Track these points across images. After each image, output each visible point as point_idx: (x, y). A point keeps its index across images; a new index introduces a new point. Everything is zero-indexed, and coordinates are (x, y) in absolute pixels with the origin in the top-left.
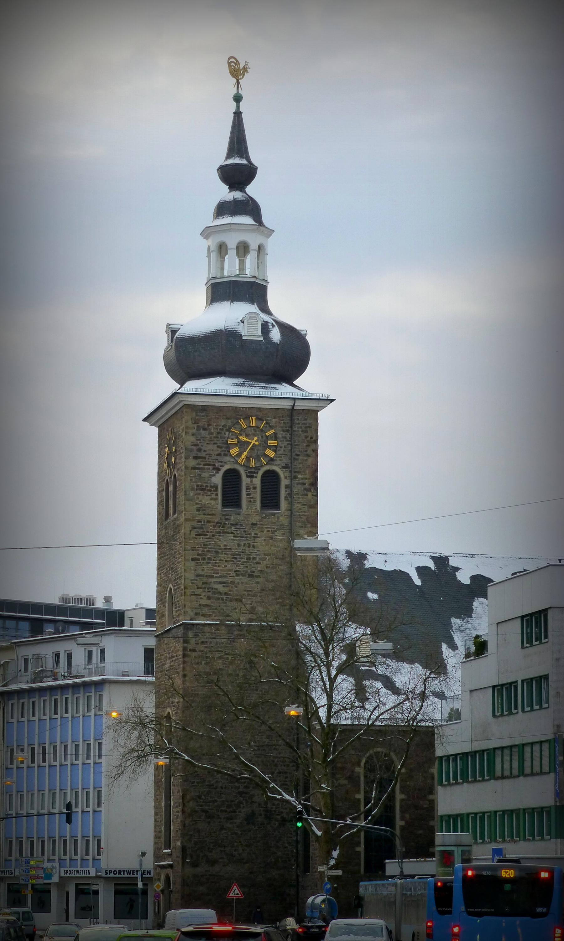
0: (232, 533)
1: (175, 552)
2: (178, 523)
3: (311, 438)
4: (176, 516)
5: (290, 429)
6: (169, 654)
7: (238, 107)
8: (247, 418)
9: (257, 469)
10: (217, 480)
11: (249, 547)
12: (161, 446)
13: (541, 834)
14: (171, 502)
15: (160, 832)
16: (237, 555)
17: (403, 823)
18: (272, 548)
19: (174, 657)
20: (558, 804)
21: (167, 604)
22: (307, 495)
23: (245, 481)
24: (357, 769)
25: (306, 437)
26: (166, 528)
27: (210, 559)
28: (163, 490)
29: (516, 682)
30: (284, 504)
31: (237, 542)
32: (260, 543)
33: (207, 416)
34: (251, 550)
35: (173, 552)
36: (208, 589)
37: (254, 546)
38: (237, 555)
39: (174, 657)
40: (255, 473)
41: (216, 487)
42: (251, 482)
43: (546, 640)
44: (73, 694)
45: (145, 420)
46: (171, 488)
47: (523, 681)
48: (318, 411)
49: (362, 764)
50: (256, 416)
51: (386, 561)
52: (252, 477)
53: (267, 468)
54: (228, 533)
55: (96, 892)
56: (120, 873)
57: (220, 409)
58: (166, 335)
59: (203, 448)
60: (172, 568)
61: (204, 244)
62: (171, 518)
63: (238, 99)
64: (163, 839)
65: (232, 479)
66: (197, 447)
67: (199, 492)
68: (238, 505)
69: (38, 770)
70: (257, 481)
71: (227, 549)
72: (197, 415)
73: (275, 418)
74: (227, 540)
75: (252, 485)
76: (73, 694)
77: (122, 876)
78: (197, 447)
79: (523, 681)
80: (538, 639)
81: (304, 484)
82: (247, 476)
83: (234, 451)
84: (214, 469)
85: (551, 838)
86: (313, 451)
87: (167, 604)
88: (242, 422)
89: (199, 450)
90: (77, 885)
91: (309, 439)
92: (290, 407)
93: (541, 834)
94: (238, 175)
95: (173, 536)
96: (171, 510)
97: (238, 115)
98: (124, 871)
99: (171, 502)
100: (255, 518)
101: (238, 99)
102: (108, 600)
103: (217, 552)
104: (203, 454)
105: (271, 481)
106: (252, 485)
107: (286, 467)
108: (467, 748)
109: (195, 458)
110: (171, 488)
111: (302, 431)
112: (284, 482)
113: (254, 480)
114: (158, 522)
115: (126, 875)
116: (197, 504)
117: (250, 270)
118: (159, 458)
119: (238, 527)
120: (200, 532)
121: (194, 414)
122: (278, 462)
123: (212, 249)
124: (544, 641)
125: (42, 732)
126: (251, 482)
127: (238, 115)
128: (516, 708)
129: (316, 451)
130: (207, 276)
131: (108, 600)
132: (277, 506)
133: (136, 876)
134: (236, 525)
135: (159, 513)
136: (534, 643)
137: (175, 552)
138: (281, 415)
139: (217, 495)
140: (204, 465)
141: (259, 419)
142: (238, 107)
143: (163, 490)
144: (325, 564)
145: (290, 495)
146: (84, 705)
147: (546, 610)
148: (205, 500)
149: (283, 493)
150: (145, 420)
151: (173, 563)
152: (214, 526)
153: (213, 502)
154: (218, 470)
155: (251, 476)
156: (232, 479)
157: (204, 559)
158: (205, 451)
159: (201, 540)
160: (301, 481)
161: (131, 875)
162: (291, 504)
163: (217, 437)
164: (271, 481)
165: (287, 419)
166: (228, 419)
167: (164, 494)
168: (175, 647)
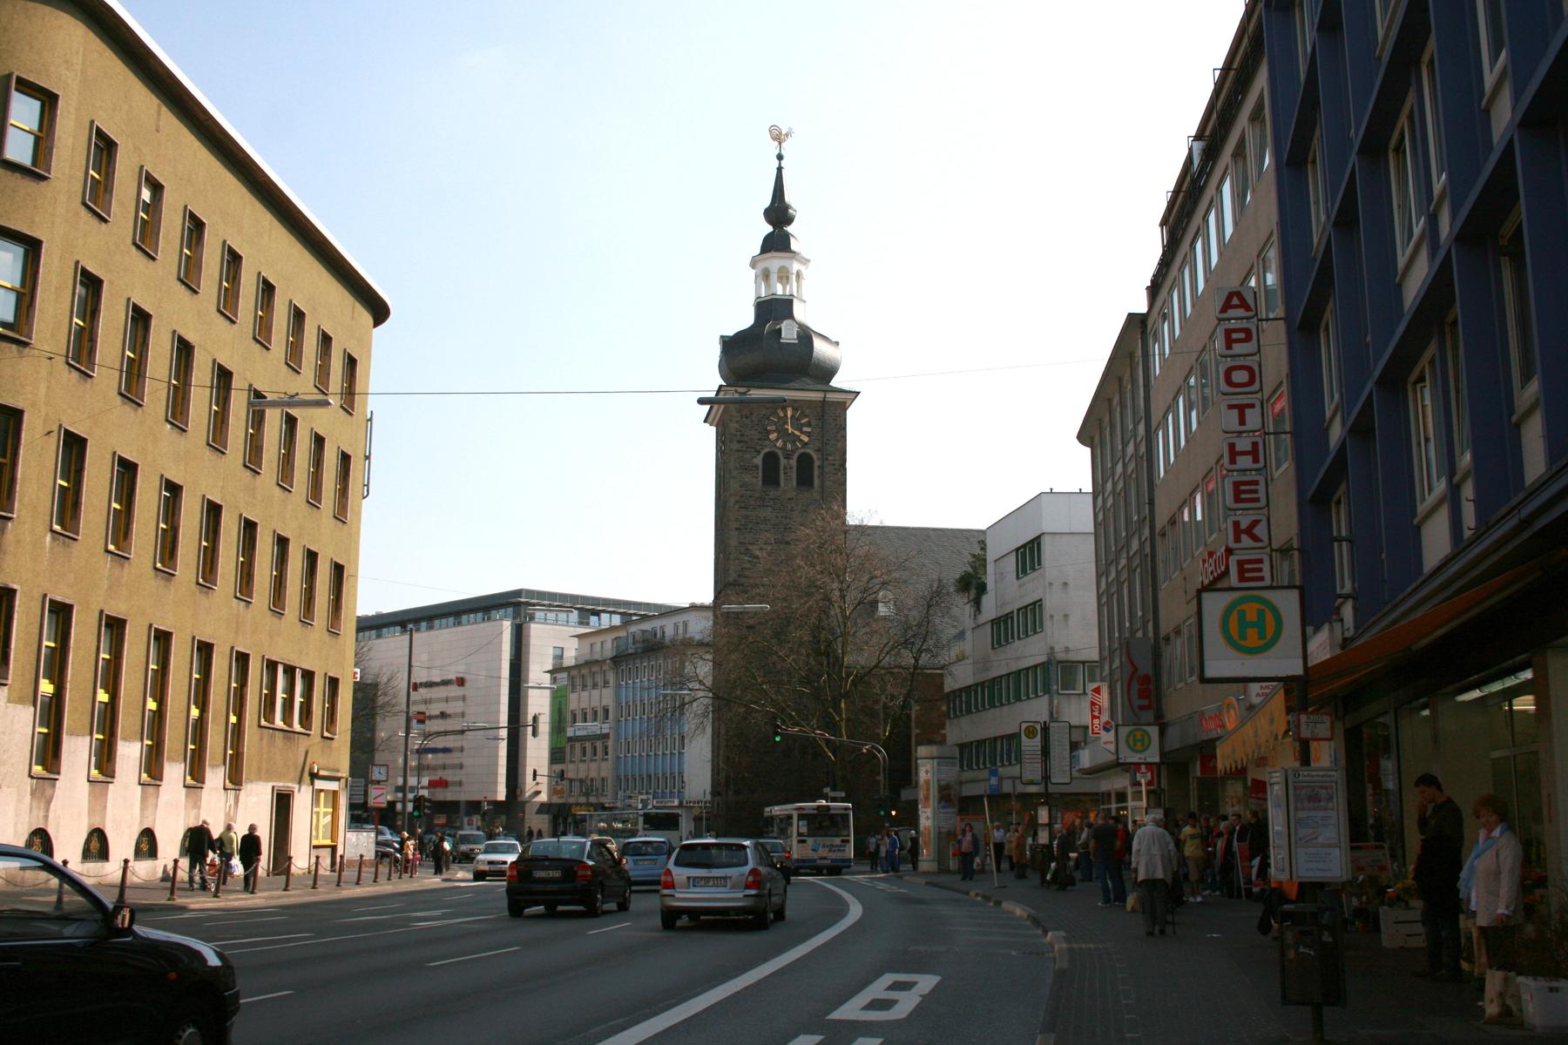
5: (821, 418)
9: (793, 451)
10: (758, 460)
13: (1009, 760)
18: (837, 593)
23: (783, 461)
30: (816, 482)
51: (1065, 584)
61: (753, 272)
65: (771, 461)
68: (777, 483)
70: (793, 462)
71: (766, 520)
74: (767, 513)
83: (773, 436)
94: (779, 214)
97: (780, 169)
100: (792, 494)
102: (65, 863)
105: (805, 463)
107: (819, 450)
108: (970, 681)
112: (817, 463)
127: (780, 169)
129: (844, 437)
131: (65, 863)
141: (795, 409)
144: (847, 530)
145: (822, 475)
148: (747, 478)
149: (816, 473)
155: (788, 457)
156: (771, 461)
159: (744, 512)
162: (822, 482)
164: (805, 463)
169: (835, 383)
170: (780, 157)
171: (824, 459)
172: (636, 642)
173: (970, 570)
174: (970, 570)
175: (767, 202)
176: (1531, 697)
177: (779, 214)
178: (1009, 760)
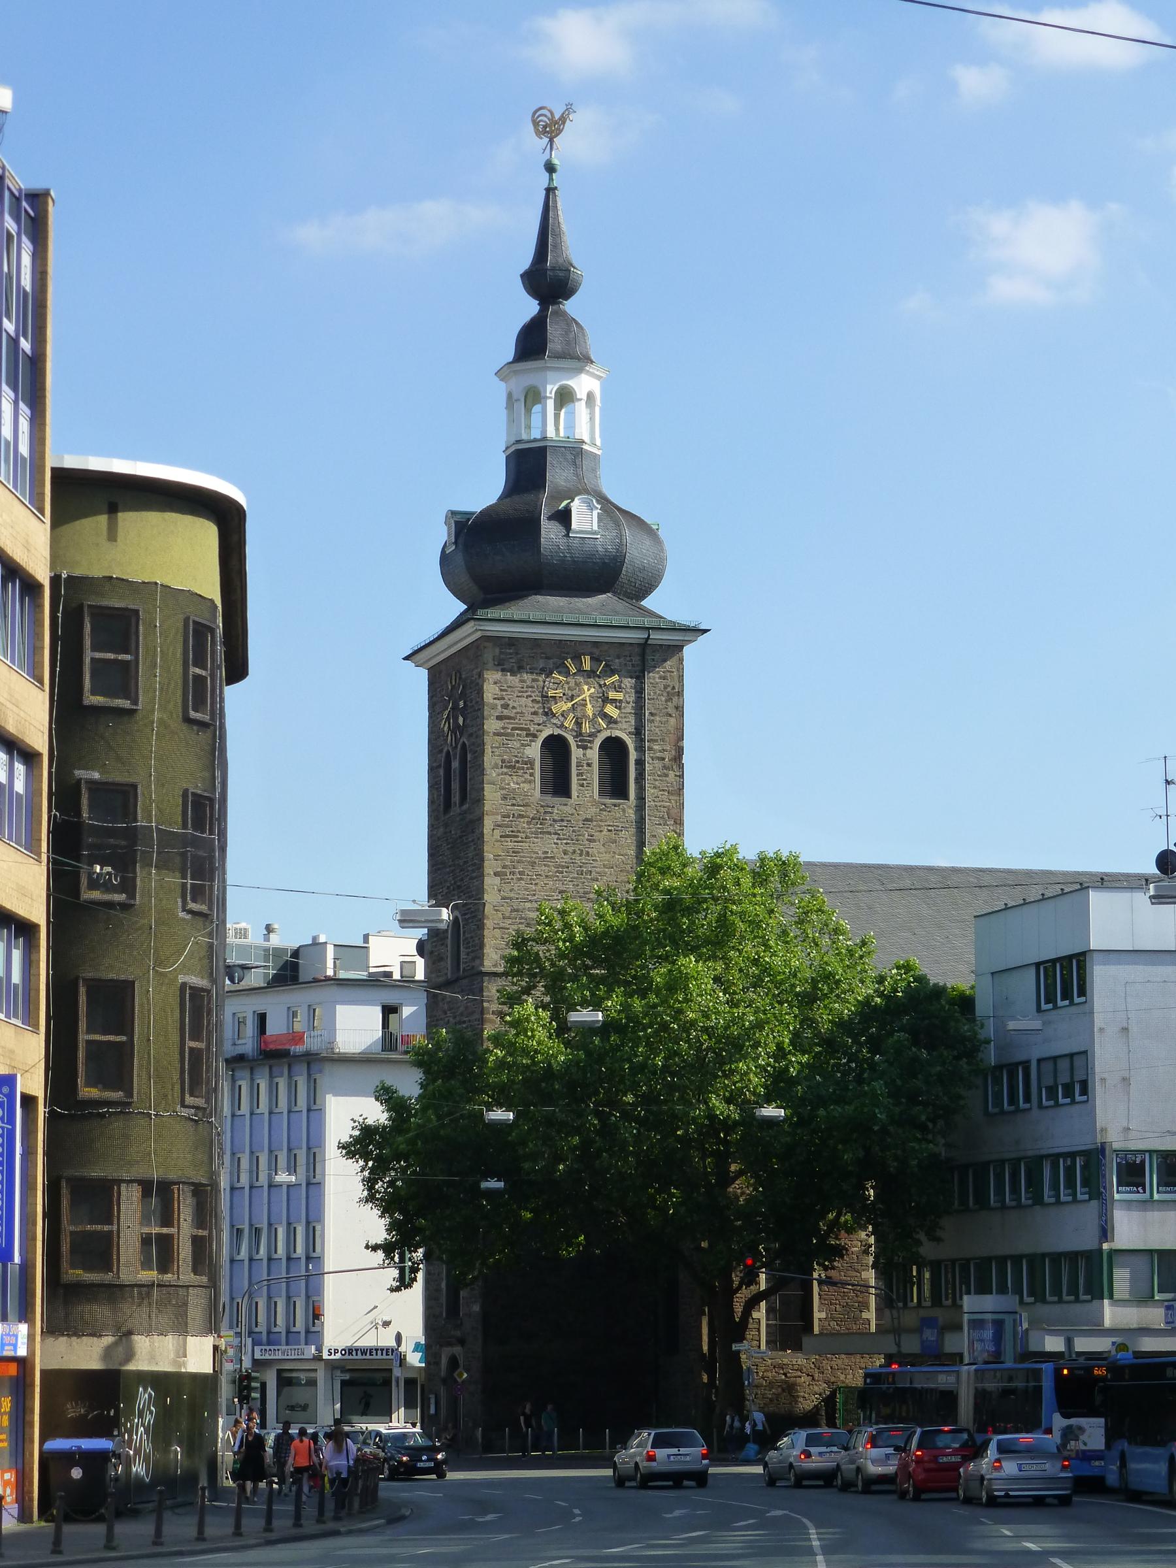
0: (556, 834)
1: (466, 862)
2: (469, 817)
3: (674, 688)
4: (465, 807)
6: (455, 1017)
8: (577, 658)
10: (534, 751)
11: (581, 855)
12: (435, 699)
13: (1056, 1290)
14: (455, 786)
15: (438, 1290)
16: (563, 867)
19: (464, 1022)
21: (449, 941)
22: (667, 776)
23: (576, 753)
25: (666, 687)
26: (446, 825)
27: (521, 873)
28: (439, 766)
31: (562, 847)
32: (596, 848)
33: (517, 654)
34: (584, 859)
35: (461, 862)
36: (521, 918)
37: (588, 853)
38: (563, 867)
39: (464, 1022)
40: (590, 742)
41: (531, 763)
42: (584, 755)
43: (1083, 999)
46: (455, 764)
48: (682, 647)
50: (590, 654)
52: (585, 748)
53: (607, 734)
54: (550, 833)
55: (312, 1383)
56: (350, 1353)
57: (536, 643)
58: (445, 528)
59: (511, 703)
60: (459, 887)
62: (455, 810)
64: (443, 1300)
65: (556, 749)
66: (503, 702)
67: (505, 770)
70: (594, 754)
72: (501, 653)
73: (618, 657)
74: (548, 844)
75: (586, 761)
77: (374, 1357)
78: (503, 702)
79: (1039, 1061)
80: (1067, 995)
81: (663, 759)
82: (578, 747)
84: (527, 735)
86: (677, 708)
87: (449, 941)
88: (569, 663)
89: (506, 706)
90: (279, 1372)
91: (669, 689)
92: (642, 641)
94: (549, 282)
95: (461, 837)
96: (456, 798)
98: (357, 1350)
99: (455, 786)
100: (592, 811)
103: (533, 864)
104: (512, 713)
106: (586, 761)
109: (499, 718)
110: (455, 764)
111: (660, 678)
112: (633, 756)
113: (588, 751)
114: (430, 816)
115: (360, 1356)
116: (503, 789)
118: (430, 717)
119: (565, 824)
120: (507, 831)
121: (497, 650)
122: (624, 726)
123: (515, 397)
124: (1077, 1000)
126: (584, 755)
127: (550, 191)
128: (1027, 1099)
130: (504, 439)
132: (624, 795)
133: (390, 1357)
134: (562, 820)
135: (431, 802)
136: (1060, 1003)
137: (466, 862)
138: (627, 653)
139: (532, 775)
140: (513, 729)
141: (596, 660)
143: (439, 766)
150: (406, 658)
151: (462, 880)
152: (529, 823)
153: (526, 786)
154: (535, 736)
156: (556, 749)
157: (514, 873)
158: (514, 707)
160: (658, 754)
161: (368, 1357)
163: (532, 687)
164: (614, 750)
165: (636, 659)
166: (548, 658)
167: (442, 772)
168: (467, 1008)
169: (647, 603)
170: (550, 168)
171: (640, 749)
172: (332, 1042)
173: (991, 1056)
174: (991, 1056)
175: (525, 260)
176: (1102, 1420)
177: (549, 282)
178: (1056, 1290)
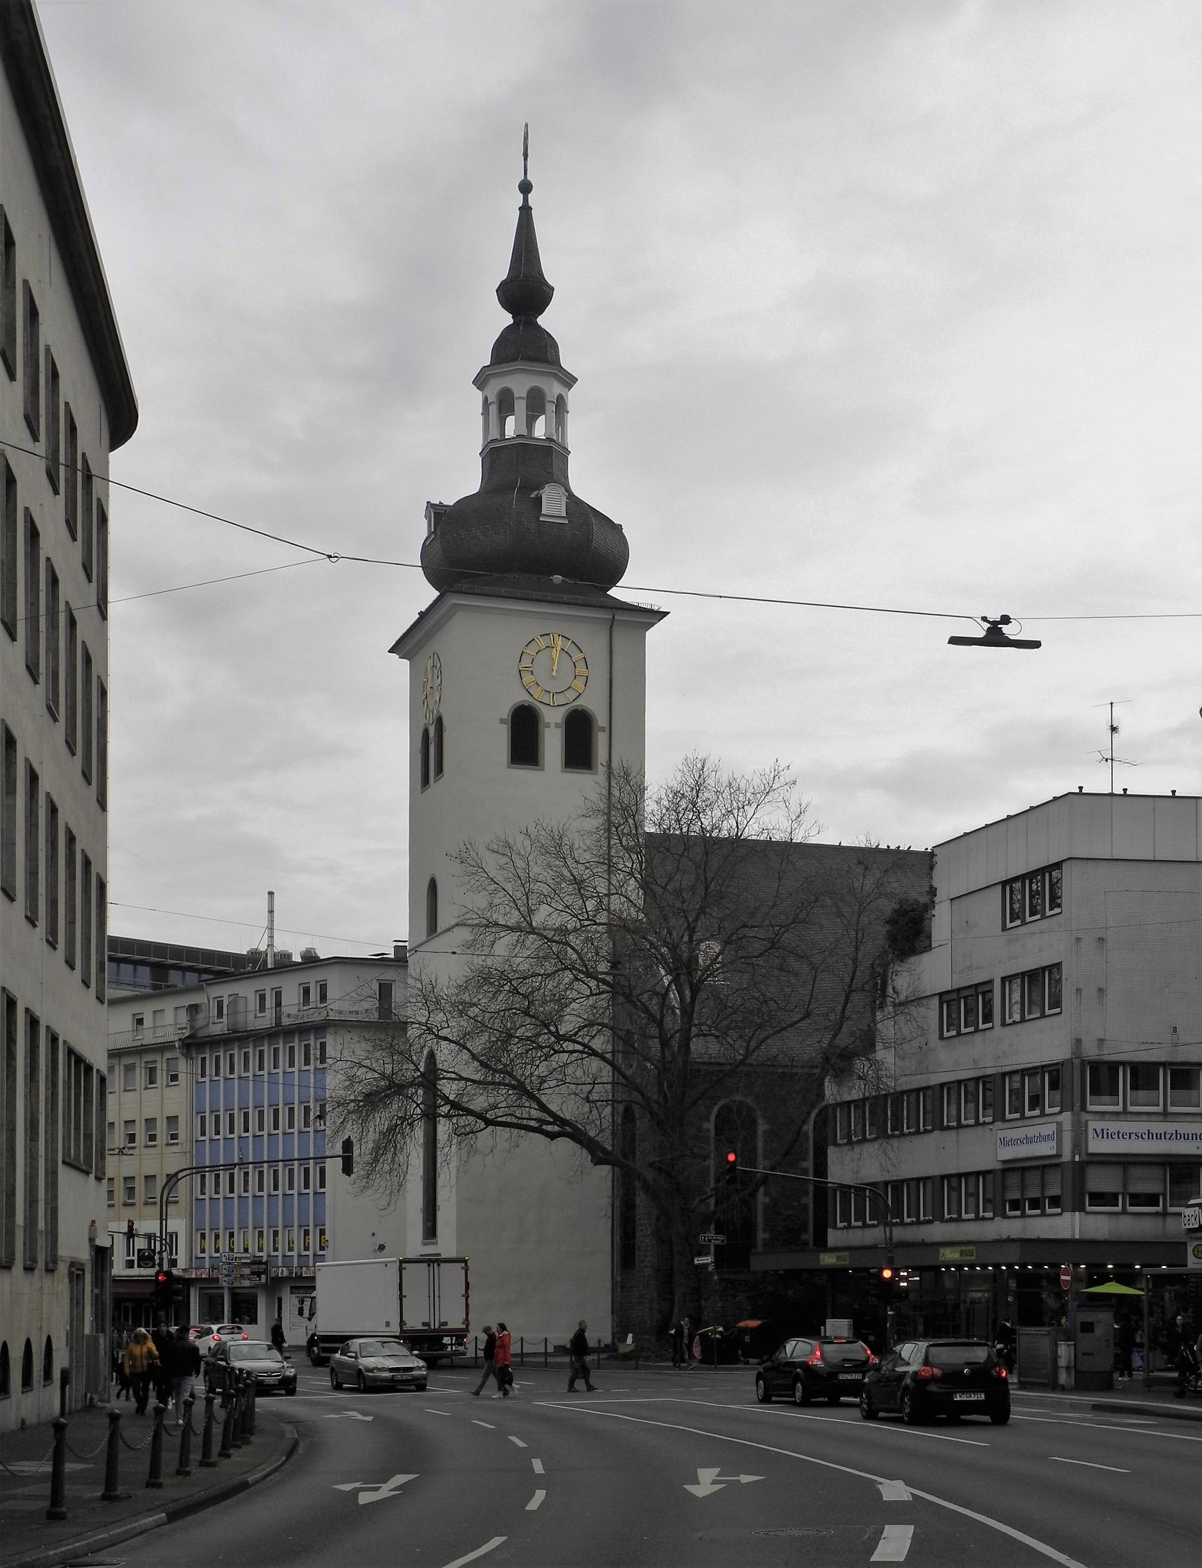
7: (526, 200)
13: (860, 1216)
17: (767, 1200)
20: (1077, 1158)
24: (706, 1125)
29: (990, 982)
44: (240, 1048)
45: (391, 651)
47: (1004, 979)
49: (713, 1117)
63: (526, 188)
69: (254, 1143)
76: (240, 1048)
79: (1004, 979)
85: (995, 1216)
93: (860, 1216)
97: (525, 211)
101: (526, 188)
117: (540, 429)
125: (258, 1091)
127: (525, 211)
142: (526, 200)
146: (299, 1056)
147: (1058, 865)
150: (391, 651)
